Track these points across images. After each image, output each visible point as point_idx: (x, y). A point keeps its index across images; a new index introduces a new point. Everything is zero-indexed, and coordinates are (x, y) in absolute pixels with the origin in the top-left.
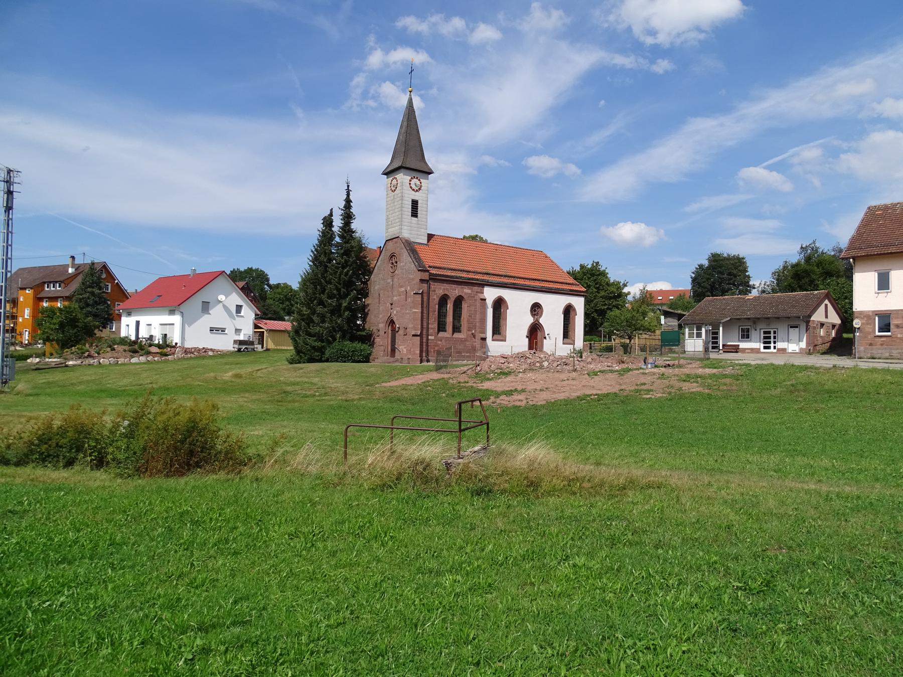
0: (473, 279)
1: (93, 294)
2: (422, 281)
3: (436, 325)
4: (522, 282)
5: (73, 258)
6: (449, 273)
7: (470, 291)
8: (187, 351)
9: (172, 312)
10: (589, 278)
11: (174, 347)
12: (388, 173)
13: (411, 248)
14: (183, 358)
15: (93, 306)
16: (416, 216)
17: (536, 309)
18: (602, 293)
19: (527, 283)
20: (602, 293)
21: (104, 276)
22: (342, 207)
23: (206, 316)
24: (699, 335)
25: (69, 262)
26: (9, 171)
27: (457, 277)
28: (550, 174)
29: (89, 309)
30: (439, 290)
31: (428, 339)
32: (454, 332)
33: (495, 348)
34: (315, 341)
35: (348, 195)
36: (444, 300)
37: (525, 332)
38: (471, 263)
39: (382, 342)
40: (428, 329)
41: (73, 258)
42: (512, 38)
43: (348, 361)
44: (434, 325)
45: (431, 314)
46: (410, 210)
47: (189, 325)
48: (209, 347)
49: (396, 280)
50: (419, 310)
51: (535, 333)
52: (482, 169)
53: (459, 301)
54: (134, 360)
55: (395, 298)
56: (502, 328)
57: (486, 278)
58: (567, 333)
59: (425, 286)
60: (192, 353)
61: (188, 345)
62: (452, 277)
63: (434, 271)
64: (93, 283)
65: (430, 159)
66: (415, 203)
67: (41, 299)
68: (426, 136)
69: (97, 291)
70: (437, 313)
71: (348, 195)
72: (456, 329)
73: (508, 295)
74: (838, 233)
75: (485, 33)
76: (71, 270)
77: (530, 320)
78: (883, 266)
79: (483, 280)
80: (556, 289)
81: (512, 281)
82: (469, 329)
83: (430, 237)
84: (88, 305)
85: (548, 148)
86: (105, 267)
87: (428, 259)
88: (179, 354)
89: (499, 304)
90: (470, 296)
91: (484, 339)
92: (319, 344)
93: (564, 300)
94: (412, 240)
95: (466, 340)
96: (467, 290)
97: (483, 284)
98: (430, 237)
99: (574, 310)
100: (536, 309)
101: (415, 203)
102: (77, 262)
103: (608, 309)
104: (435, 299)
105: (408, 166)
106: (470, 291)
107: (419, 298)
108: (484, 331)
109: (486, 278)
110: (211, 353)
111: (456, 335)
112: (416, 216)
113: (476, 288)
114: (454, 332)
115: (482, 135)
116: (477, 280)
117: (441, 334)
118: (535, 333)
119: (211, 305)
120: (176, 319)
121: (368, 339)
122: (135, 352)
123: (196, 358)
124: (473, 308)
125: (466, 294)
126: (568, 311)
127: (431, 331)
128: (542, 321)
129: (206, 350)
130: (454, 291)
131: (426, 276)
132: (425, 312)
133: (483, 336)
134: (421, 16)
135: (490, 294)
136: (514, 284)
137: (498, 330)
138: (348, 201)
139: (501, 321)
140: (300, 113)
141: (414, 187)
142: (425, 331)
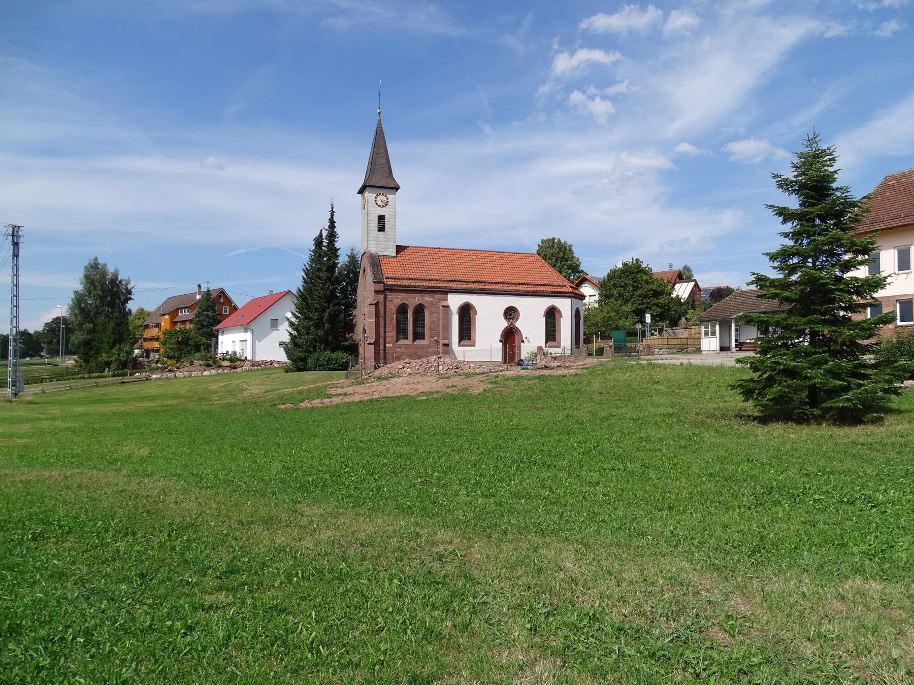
0: (433, 287)
1: (207, 315)
2: (377, 292)
3: (394, 333)
5: (199, 286)
7: (431, 299)
8: (254, 364)
9: (246, 330)
12: (361, 192)
13: (376, 261)
14: (250, 370)
15: (208, 327)
17: (511, 313)
18: (639, 292)
19: (499, 287)
20: (639, 292)
21: (222, 300)
22: (327, 227)
23: (275, 332)
24: (714, 333)
25: (196, 290)
26: (14, 227)
27: (415, 286)
28: (758, 160)
29: (204, 330)
30: (396, 300)
31: (385, 347)
32: (415, 339)
33: (460, 352)
34: (301, 352)
35: (332, 216)
37: (498, 335)
38: (437, 273)
39: (367, 352)
40: (385, 337)
41: (199, 286)
42: (709, 20)
43: (324, 369)
44: (391, 333)
50: (373, 320)
51: (510, 337)
52: (681, 160)
53: (420, 310)
54: (206, 373)
57: (450, 285)
58: (551, 334)
59: (381, 297)
61: (258, 358)
62: (410, 286)
63: (390, 282)
64: (209, 307)
65: (399, 175)
66: (381, 220)
67: (176, 323)
69: (210, 314)
70: (394, 321)
71: (332, 216)
72: (419, 335)
73: (474, 300)
75: (681, 20)
76: (198, 297)
77: (505, 324)
78: (902, 242)
79: (445, 288)
80: (533, 291)
81: (481, 286)
82: (431, 336)
83: (400, 249)
84: (203, 326)
85: (752, 131)
86: (222, 293)
87: (390, 271)
88: (247, 366)
89: (466, 312)
90: (431, 304)
92: (302, 355)
93: (545, 303)
96: (428, 298)
97: (446, 292)
98: (400, 249)
99: (559, 311)
100: (511, 313)
101: (381, 220)
102: (202, 290)
103: (647, 308)
104: (392, 308)
105: (371, 184)
106: (431, 299)
107: (373, 308)
108: (448, 335)
109: (450, 285)
110: (276, 365)
111: (418, 342)
113: (438, 296)
114: (415, 339)
115: (674, 128)
116: (439, 287)
118: (510, 337)
119: (279, 322)
120: (248, 336)
121: (353, 349)
122: (209, 366)
124: (435, 315)
125: (427, 301)
126: (552, 315)
127: (388, 339)
128: (518, 324)
129: (272, 363)
130: (413, 301)
131: (381, 287)
133: (446, 342)
134: (610, 12)
135: (455, 301)
136: (482, 289)
137: (466, 334)
138: (332, 222)
140: (488, 129)
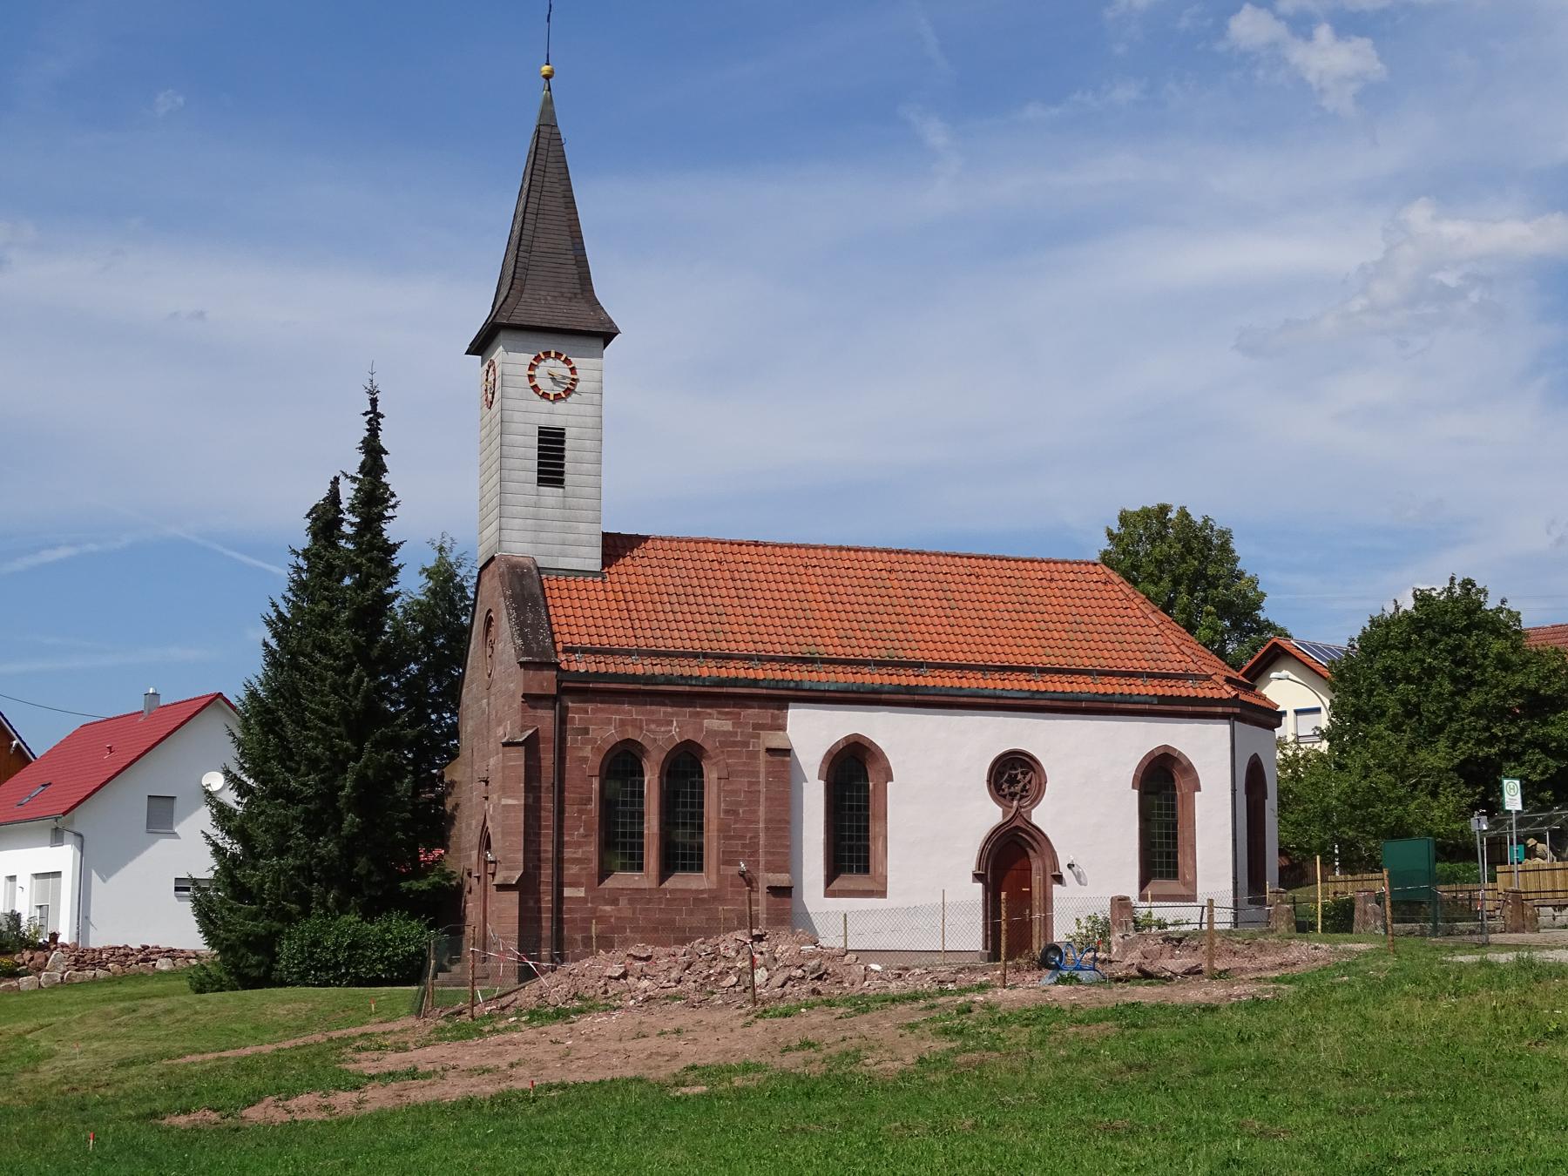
0: (735, 682)
4: (949, 680)
6: (640, 667)
7: (727, 725)
8: (82, 958)
9: (57, 837)
10: (1433, 642)
11: (44, 947)
16: (559, 483)
17: (1014, 775)
27: (669, 680)
30: (601, 727)
31: (559, 898)
33: (834, 918)
35: (374, 430)
36: (623, 762)
38: (749, 630)
40: (559, 862)
43: (338, 981)
44: (583, 849)
45: (570, 811)
46: (534, 464)
47: (106, 874)
48: (164, 946)
53: (685, 765)
56: (875, 847)
59: (546, 718)
60: (102, 965)
62: (651, 680)
63: (581, 665)
65: (613, 288)
66: (551, 445)
68: (596, 203)
70: (594, 806)
71: (374, 430)
77: (991, 814)
79: (776, 684)
80: (1095, 698)
81: (906, 679)
82: (728, 859)
83: (616, 547)
87: (579, 623)
88: (57, 967)
89: (853, 770)
91: (783, 892)
93: (1138, 739)
94: (543, 562)
95: (716, 897)
96: (716, 723)
97: (781, 698)
99: (1189, 770)
100: (1014, 775)
101: (551, 445)
104: (586, 756)
105: (516, 320)
106: (727, 725)
107: (517, 757)
109: (796, 674)
110: (163, 964)
111: (680, 881)
112: (559, 483)
113: (752, 714)
116: (755, 683)
117: (621, 880)
119: (178, 804)
120: (63, 857)
121: (444, 908)
123: (113, 980)
124: (742, 783)
125: (712, 733)
126: (1162, 781)
127: (571, 870)
128: (1040, 816)
130: (663, 730)
131: (546, 682)
132: (548, 803)
133: (781, 879)
135: (812, 733)
136: (909, 689)
137: (853, 853)
139: (874, 828)
141: (545, 385)
142: (546, 873)
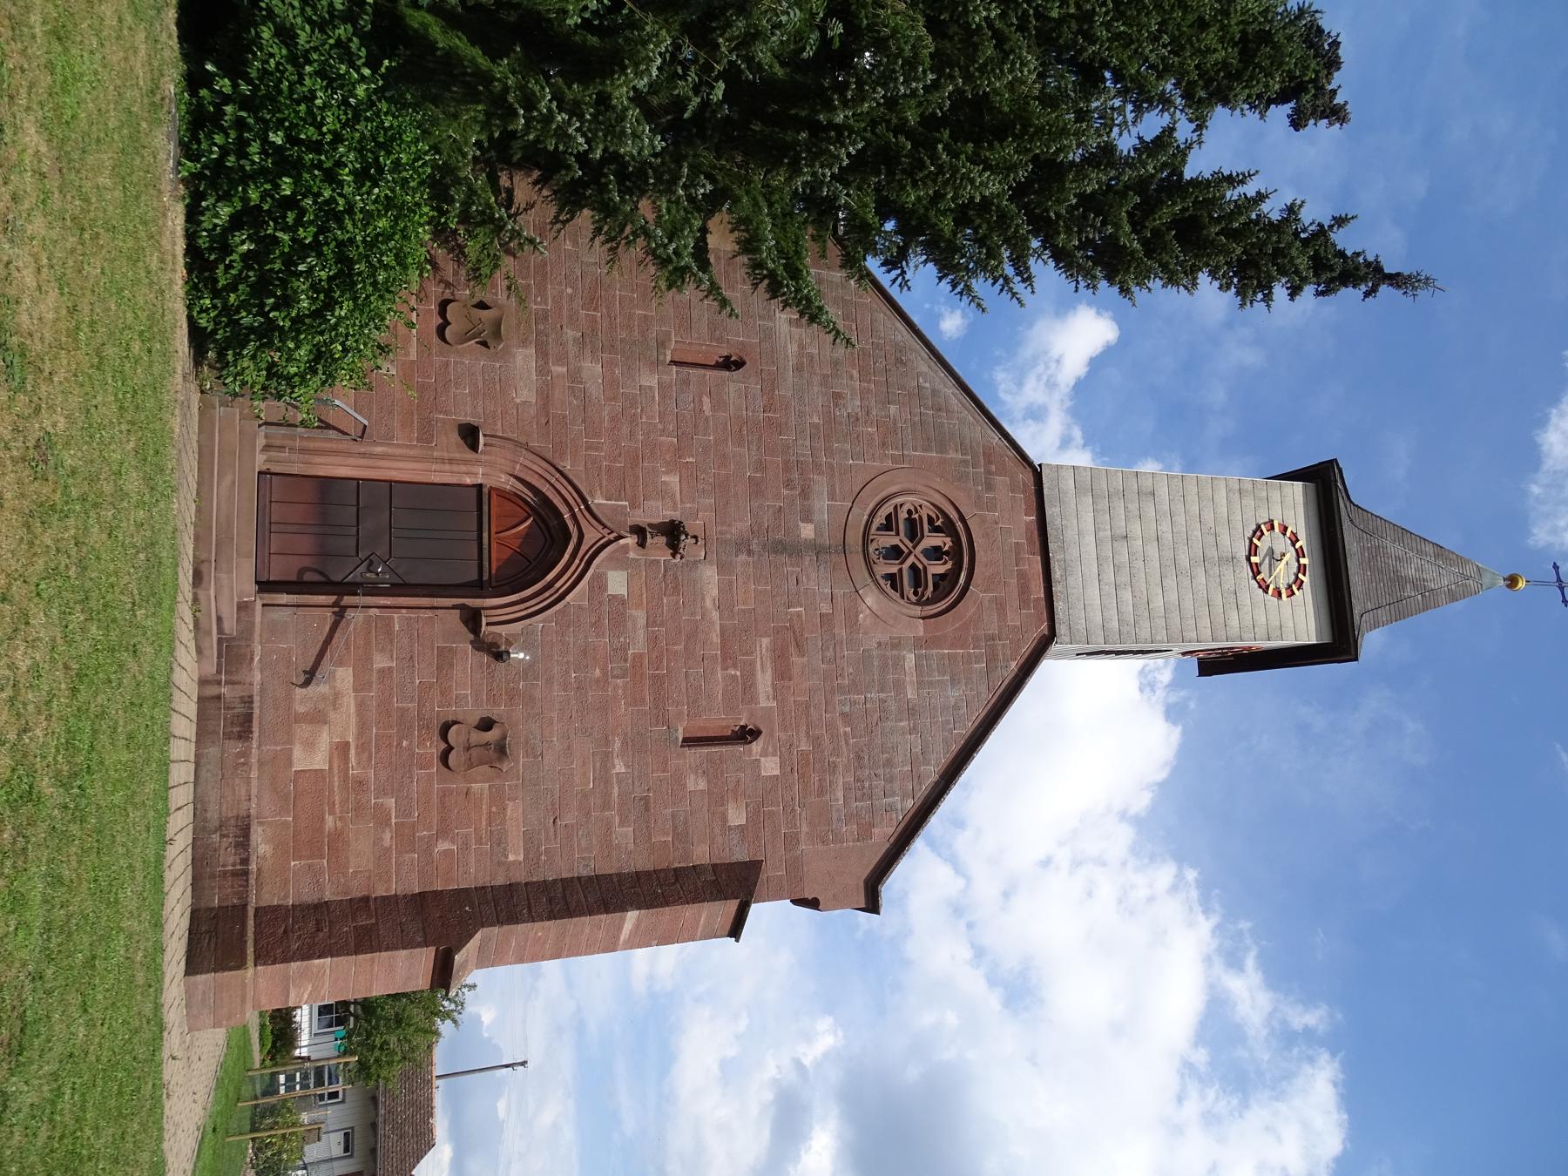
49: (819, 584)
55: (709, 576)
74: (1389, 269)
